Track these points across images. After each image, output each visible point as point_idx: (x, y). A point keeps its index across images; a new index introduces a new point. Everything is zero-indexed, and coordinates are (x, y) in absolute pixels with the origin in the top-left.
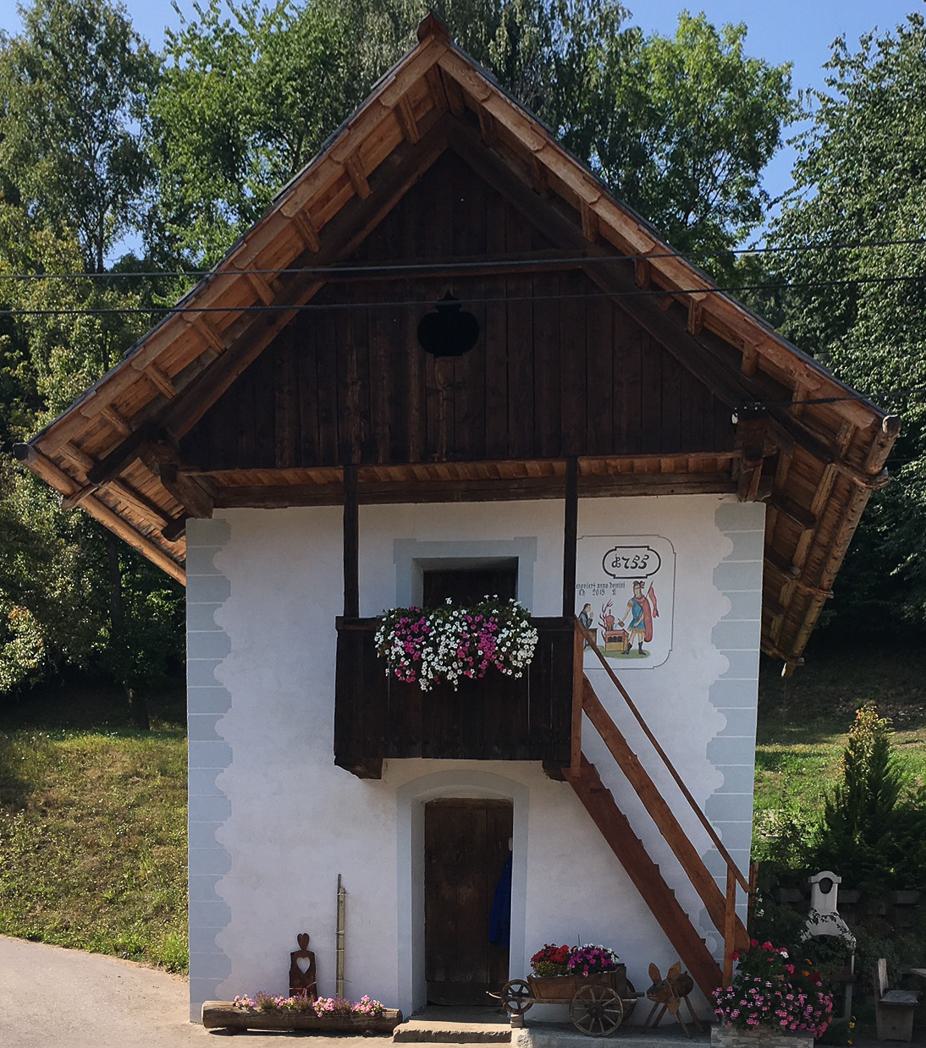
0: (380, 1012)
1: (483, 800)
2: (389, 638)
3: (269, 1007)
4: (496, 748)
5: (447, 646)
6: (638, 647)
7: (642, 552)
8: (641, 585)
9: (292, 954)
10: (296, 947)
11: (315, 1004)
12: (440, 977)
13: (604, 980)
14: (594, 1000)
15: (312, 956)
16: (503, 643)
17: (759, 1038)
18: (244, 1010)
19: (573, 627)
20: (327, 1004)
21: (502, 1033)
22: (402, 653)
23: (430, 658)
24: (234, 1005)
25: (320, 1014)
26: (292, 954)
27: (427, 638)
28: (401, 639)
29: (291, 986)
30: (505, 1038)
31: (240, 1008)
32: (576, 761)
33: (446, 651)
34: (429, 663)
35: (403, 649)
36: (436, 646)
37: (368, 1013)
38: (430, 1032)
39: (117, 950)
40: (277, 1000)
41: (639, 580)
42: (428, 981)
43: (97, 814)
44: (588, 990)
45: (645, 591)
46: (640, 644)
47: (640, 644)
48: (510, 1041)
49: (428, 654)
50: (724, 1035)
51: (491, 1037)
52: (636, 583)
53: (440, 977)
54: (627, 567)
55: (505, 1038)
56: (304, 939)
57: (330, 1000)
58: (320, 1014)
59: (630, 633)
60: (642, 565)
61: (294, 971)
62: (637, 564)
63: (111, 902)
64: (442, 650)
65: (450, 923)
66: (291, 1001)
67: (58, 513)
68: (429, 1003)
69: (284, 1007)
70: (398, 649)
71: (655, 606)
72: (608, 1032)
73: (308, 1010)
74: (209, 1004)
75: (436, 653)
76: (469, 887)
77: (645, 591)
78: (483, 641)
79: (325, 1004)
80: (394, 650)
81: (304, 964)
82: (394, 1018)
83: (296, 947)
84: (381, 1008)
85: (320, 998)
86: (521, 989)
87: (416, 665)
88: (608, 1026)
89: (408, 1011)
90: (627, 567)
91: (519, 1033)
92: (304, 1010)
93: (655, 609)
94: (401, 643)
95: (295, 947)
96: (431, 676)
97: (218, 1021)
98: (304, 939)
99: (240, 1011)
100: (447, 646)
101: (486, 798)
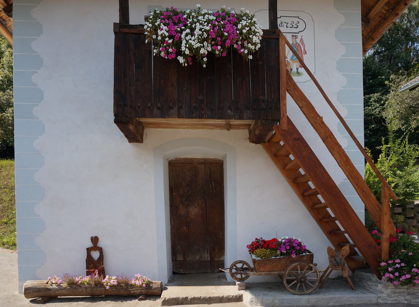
0: (148, 284)
1: (204, 159)
2: (156, 24)
3: (72, 284)
4: (229, 112)
5: (201, 30)
6: (296, 70)
7: (296, 20)
8: (296, 37)
9: (87, 249)
10: (90, 245)
11: (104, 281)
12: (180, 258)
13: (305, 259)
14: (299, 272)
15: (101, 250)
16: (243, 28)
17: (407, 289)
18: (54, 286)
19: (279, 35)
20: (112, 281)
21: (236, 296)
22: (167, 34)
23: (188, 38)
24: (47, 283)
25: (108, 287)
26: (87, 249)
27: (186, 25)
28: (165, 25)
29: (87, 268)
30: (239, 299)
31: (51, 285)
32: (284, 120)
33: (200, 33)
34: (187, 41)
35: (167, 32)
36: (193, 30)
37: (141, 286)
38: (186, 298)
39: (4, 245)
40: (77, 279)
41: (295, 34)
42: (172, 260)
43: (4, 188)
44: (296, 266)
45: (298, 40)
46: (297, 69)
47: (297, 69)
48: (242, 301)
49: (187, 35)
50: (386, 289)
51: (229, 299)
52: (293, 36)
53: (180, 258)
54: (287, 27)
55: (239, 299)
56: (95, 240)
57: (114, 278)
58: (108, 287)
59: (291, 62)
60: (296, 26)
61: (90, 261)
62: (293, 26)
63: (6, 223)
64: (197, 32)
65: (185, 228)
66: (87, 279)
67: (7, 98)
68: (174, 273)
69: (83, 283)
70: (163, 31)
71: (304, 48)
72: (309, 292)
73: (99, 284)
74: (29, 283)
75: (192, 34)
76: (196, 207)
77: (298, 40)
78: (228, 27)
79: (110, 280)
80: (160, 32)
81: (96, 255)
82: (159, 288)
83: (90, 245)
84: (149, 281)
85: (107, 277)
86: (243, 266)
87: (178, 44)
88: (308, 287)
89: (165, 281)
90: (287, 27)
91: (247, 296)
92: (96, 285)
93: (305, 50)
94: (165, 28)
95: (90, 245)
96: (187, 52)
97: (35, 294)
98: (95, 240)
99: (51, 287)
100: (201, 30)
101: (205, 158)
